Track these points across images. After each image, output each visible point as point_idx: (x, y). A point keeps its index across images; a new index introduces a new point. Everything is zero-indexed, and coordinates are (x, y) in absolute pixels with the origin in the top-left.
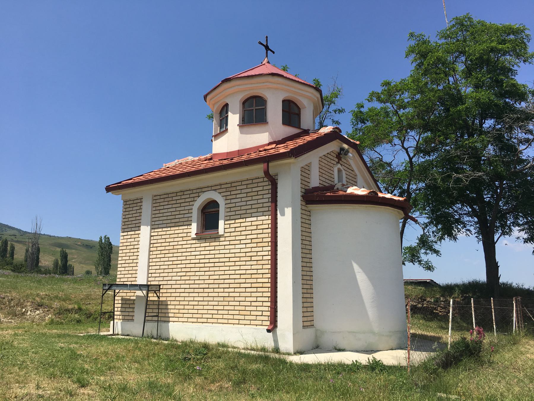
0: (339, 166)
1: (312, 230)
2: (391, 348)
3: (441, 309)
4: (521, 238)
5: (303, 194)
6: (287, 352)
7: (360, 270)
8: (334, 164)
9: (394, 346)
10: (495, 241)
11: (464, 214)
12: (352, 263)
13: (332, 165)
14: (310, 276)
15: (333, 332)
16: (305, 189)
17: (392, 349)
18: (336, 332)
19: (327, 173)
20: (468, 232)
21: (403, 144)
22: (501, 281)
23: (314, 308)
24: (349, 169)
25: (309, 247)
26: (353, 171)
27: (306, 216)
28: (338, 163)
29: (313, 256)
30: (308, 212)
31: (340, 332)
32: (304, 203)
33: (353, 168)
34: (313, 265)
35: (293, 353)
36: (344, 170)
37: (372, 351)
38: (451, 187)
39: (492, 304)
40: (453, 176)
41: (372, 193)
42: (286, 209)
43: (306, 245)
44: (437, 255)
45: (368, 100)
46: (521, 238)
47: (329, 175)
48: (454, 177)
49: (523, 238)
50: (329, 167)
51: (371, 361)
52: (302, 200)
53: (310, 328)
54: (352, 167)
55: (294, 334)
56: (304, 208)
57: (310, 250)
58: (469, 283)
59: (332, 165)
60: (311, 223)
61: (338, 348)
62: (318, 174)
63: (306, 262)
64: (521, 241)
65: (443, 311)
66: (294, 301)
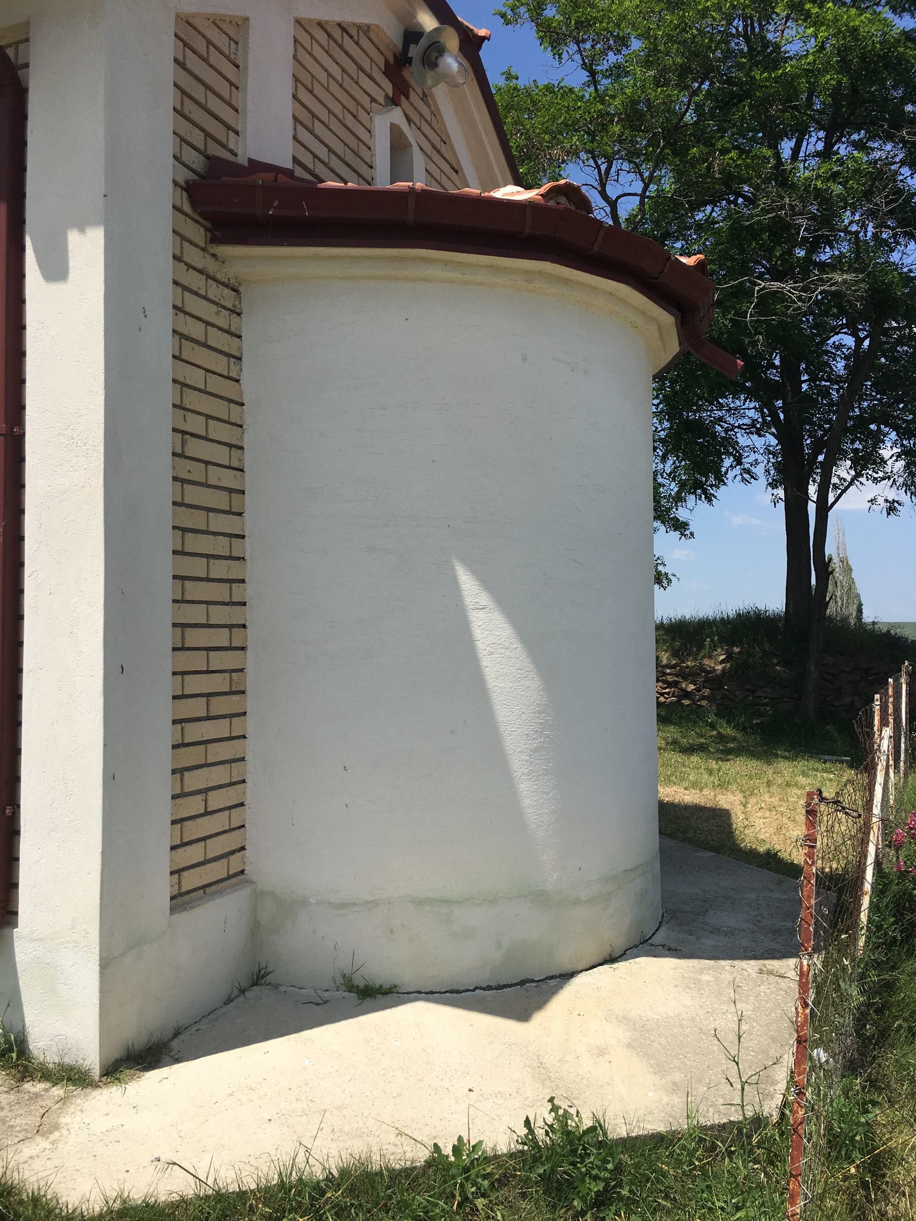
0: (396, 116)
1: (249, 388)
2: (606, 956)
3: (665, 688)
4: (881, 500)
5: (191, 176)
6: (67, 1060)
7: (484, 599)
8: (373, 100)
9: (616, 936)
10: (830, 502)
11: (739, 427)
12: (453, 569)
13: (366, 101)
14: (230, 627)
15: (343, 906)
16: (208, 157)
17: (611, 960)
18: (354, 904)
19: (335, 125)
20: (746, 476)
21: (603, 185)
22: (831, 610)
23: (249, 784)
24: (439, 152)
25: (228, 479)
26: (457, 172)
27: (214, 308)
28: (394, 101)
29: (250, 524)
30: (227, 291)
31: (373, 904)
32: (197, 233)
33: (458, 161)
34: (251, 571)
35: (96, 1072)
36: (421, 149)
37: (522, 983)
38: (751, 321)
39: (891, 700)
40: (757, 288)
41: (563, 200)
42: (74, 238)
43: (207, 463)
44: (682, 534)
45: (503, 16)
46: (881, 500)
47: (353, 143)
48: (759, 291)
49: (886, 501)
50: (351, 105)
51: (540, 1133)
52: (187, 208)
53: (220, 893)
54: (453, 148)
55: (104, 965)
56: (194, 256)
57: (231, 491)
58: (739, 615)
59: (366, 101)
60: (240, 349)
61: (359, 982)
62: (285, 108)
63: (208, 556)
64: (881, 507)
65: (668, 693)
66: (110, 778)
